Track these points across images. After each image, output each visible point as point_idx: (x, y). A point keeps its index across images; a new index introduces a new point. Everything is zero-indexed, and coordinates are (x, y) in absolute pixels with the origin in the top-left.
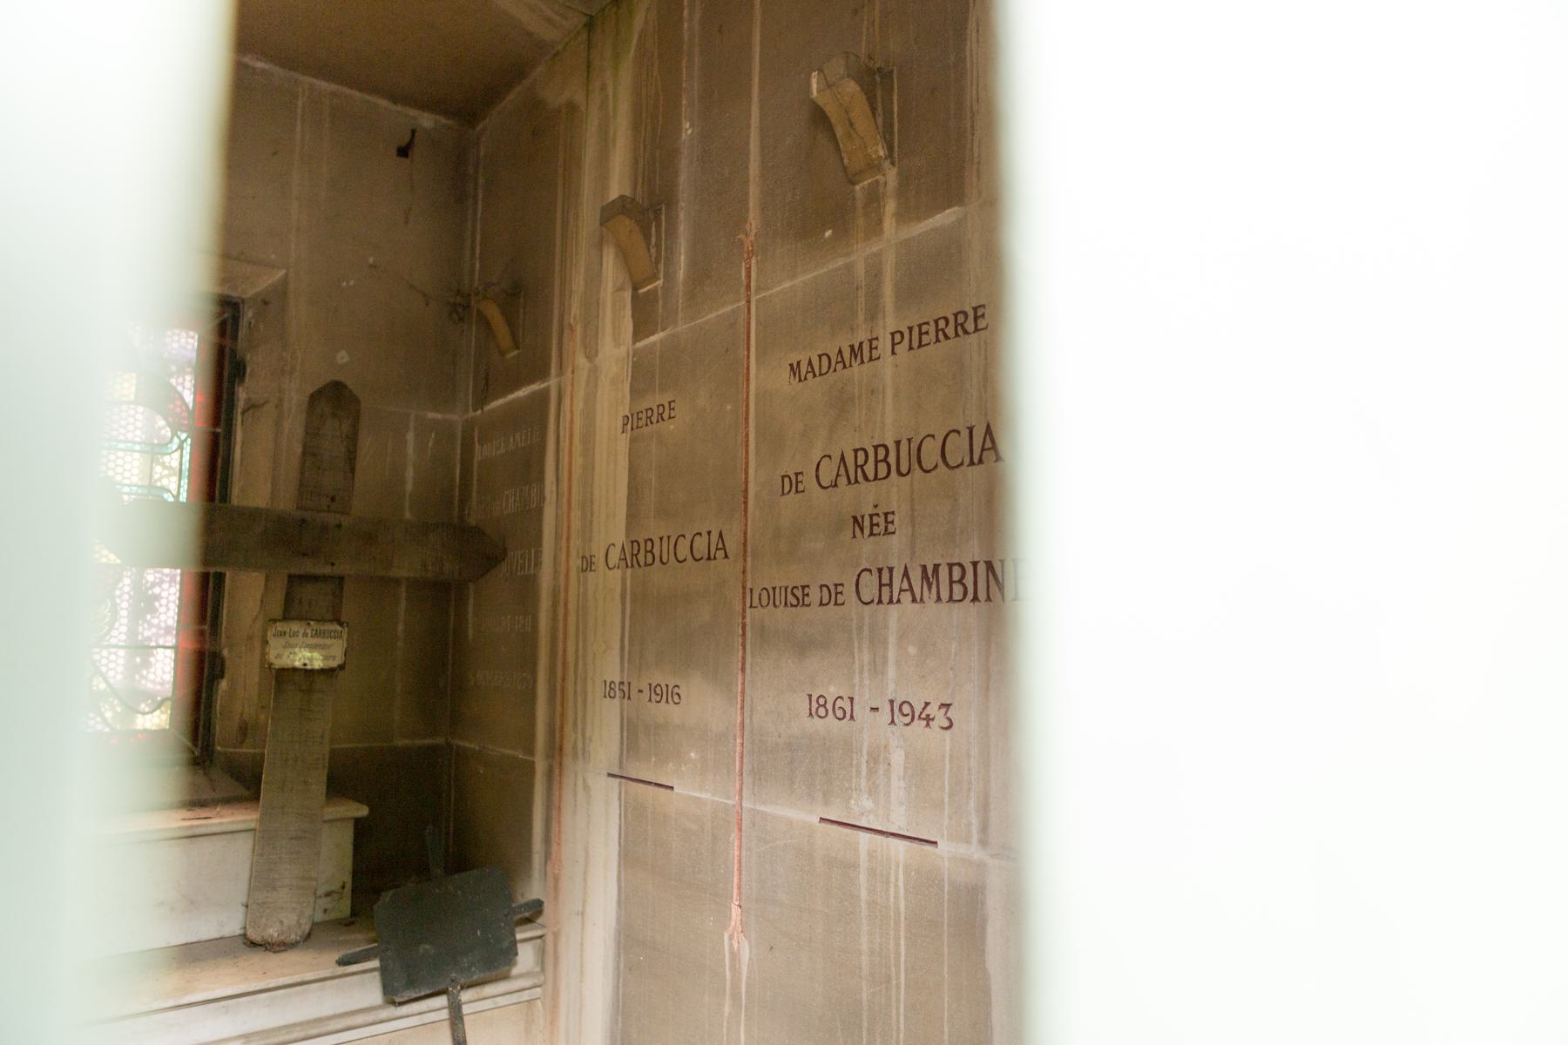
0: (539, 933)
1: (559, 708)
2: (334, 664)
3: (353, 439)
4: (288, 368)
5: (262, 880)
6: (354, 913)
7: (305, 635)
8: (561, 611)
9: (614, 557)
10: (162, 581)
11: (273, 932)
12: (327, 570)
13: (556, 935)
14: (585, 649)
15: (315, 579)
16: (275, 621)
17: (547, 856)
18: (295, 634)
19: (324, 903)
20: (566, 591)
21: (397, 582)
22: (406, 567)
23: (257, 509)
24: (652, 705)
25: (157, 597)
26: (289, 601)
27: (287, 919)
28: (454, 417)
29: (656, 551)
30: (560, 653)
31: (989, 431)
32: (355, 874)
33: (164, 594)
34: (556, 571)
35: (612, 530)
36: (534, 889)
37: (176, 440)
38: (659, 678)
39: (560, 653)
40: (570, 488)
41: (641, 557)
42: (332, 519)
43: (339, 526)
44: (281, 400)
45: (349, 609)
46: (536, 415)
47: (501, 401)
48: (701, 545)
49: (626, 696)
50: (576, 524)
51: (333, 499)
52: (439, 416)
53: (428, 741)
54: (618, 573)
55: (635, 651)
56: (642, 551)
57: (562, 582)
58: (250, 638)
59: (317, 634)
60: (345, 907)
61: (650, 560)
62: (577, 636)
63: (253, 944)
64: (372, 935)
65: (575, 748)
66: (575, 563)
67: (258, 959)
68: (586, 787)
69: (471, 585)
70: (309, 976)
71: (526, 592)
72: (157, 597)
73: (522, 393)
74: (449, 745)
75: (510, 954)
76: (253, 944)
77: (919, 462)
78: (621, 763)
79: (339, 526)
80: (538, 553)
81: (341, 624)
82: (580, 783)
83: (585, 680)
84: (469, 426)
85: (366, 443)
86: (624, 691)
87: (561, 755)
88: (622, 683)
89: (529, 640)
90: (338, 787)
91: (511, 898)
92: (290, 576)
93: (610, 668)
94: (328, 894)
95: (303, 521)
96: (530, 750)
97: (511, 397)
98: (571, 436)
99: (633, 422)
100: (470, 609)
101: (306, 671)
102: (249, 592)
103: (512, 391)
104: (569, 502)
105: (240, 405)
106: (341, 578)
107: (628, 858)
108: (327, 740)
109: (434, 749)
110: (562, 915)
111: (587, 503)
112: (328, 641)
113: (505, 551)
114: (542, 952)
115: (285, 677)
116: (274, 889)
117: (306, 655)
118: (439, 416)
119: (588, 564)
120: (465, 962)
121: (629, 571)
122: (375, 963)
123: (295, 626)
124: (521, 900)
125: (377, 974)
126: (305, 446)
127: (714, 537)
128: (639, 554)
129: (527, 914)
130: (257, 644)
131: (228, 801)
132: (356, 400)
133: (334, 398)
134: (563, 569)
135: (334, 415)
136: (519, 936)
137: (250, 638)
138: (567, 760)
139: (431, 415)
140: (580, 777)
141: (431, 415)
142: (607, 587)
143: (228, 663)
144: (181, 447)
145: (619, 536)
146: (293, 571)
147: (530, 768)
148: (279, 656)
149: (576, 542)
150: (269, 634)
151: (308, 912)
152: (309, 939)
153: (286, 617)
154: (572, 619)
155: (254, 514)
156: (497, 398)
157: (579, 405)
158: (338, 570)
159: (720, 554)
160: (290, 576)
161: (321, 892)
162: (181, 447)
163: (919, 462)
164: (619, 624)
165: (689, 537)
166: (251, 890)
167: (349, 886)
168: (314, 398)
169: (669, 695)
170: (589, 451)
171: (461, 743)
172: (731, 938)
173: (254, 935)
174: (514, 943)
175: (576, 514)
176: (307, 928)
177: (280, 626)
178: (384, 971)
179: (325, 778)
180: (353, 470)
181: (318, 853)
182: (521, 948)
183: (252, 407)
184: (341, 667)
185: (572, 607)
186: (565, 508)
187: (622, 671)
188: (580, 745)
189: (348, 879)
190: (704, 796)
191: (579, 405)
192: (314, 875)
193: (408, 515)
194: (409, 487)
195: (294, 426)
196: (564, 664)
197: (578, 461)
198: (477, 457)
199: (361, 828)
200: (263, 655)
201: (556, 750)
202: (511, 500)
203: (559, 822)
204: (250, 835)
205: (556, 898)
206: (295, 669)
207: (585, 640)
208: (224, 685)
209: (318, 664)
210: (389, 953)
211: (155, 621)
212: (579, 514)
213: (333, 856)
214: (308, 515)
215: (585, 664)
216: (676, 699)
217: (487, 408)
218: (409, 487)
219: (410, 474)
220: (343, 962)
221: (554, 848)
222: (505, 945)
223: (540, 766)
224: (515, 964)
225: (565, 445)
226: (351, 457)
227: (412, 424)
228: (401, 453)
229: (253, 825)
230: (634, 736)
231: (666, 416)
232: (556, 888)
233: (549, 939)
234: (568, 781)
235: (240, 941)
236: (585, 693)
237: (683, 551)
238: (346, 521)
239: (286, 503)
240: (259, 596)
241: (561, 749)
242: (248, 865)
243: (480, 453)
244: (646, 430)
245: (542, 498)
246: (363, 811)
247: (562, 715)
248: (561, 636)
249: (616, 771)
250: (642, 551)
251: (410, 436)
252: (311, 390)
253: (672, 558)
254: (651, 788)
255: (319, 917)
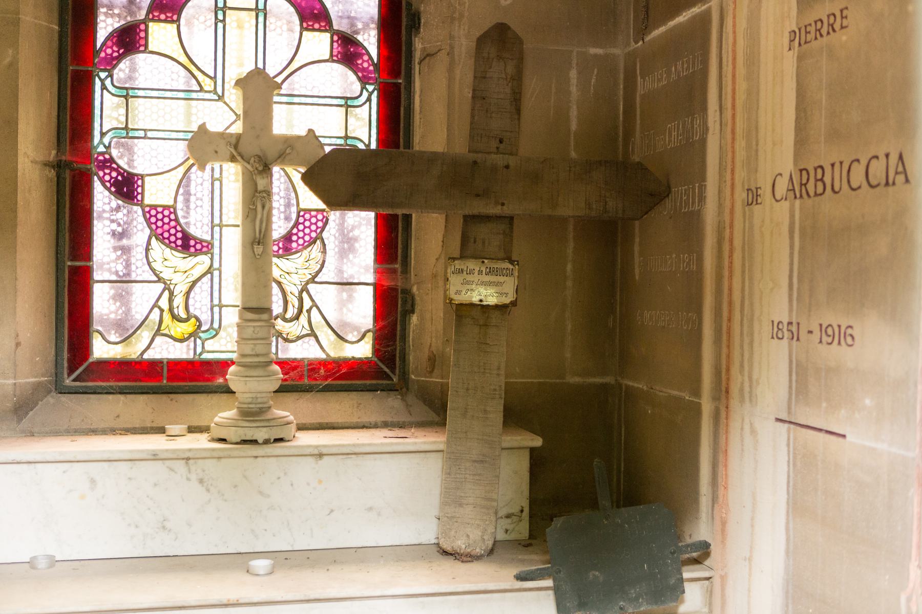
0: (706, 574)
1: (724, 350)
2: (507, 300)
3: (518, 78)
4: (457, 15)
5: (451, 498)
6: (531, 536)
7: (480, 272)
8: (726, 247)
9: (782, 186)
10: (360, 224)
11: (460, 544)
12: (497, 210)
13: (723, 578)
14: (751, 288)
15: (487, 218)
16: (454, 259)
17: (714, 500)
18: (471, 272)
19: (505, 523)
20: (731, 226)
21: (564, 220)
22: (573, 205)
23: (435, 154)
24: (823, 348)
25: (356, 239)
26: (465, 240)
27: (473, 534)
28: (616, 51)
29: (828, 179)
30: (726, 291)
31: (901, 157)
32: (533, 502)
33: (362, 236)
34: (720, 206)
35: (779, 159)
36: (701, 531)
37: (365, 94)
38: (830, 318)
39: (726, 291)
40: (734, 116)
41: (811, 187)
42: (499, 160)
43: (507, 167)
44: (452, 47)
45: (520, 249)
46: (698, 37)
47: (662, 29)
48: (877, 169)
49: (795, 337)
50: (741, 155)
51: (501, 141)
52: (599, 51)
53: (598, 380)
54: (786, 205)
55: (804, 289)
56: (812, 180)
57: (727, 219)
58: (435, 276)
59: (490, 272)
60: (523, 530)
61: (820, 189)
62: (743, 272)
63: (445, 553)
64: (547, 557)
65: (741, 390)
66: (741, 196)
67: (449, 565)
68: (753, 432)
69: (637, 223)
70: (491, 586)
71: (691, 225)
72: (356, 239)
73: (682, 18)
74: (620, 385)
75: (676, 591)
76: (445, 553)
77: (849, 181)
78: (789, 408)
79: (507, 167)
80: (703, 188)
81: (512, 262)
82: (747, 427)
83: (751, 321)
84: (631, 57)
85: (532, 86)
86: (792, 331)
87: (727, 398)
88: (790, 323)
89: (695, 279)
90: (514, 417)
91: (679, 538)
92: (466, 218)
93: (775, 304)
94: (508, 516)
95: (475, 162)
96: (697, 392)
97: (672, 24)
98: (734, 59)
99: (800, 37)
100: (636, 248)
101: (482, 306)
102: (431, 233)
103: (672, 17)
104: (733, 132)
105: (417, 55)
106: (511, 218)
107: (797, 507)
108: (502, 372)
109: (604, 386)
110: (729, 557)
111: (753, 130)
112: (501, 279)
113: (669, 187)
114: (710, 593)
115: (464, 312)
116: (461, 505)
117: (486, 294)
118: (599, 51)
119: (754, 197)
120: (633, 593)
121: (798, 202)
122: (549, 583)
123: (471, 264)
124: (689, 541)
125: (551, 593)
126: (474, 90)
127: (894, 159)
128: (809, 183)
129: (695, 555)
130: (441, 283)
131: (422, 425)
132: (519, 41)
133: (499, 40)
134: (728, 203)
135: (499, 58)
136: (686, 575)
137: (435, 276)
138: (734, 403)
139: (593, 51)
140: (747, 421)
141: (593, 51)
142: (776, 218)
143: (417, 299)
144: (369, 99)
145: (787, 165)
146: (467, 212)
147: (696, 410)
148: (458, 292)
149: (740, 174)
150: (449, 271)
151: (491, 529)
152: (491, 552)
153: (462, 257)
154: (737, 255)
155: (433, 158)
156: (657, 27)
157: (742, 24)
158: (507, 210)
159: (901, 178)
160: (466, 218)
161: (502, 513)
162: (369, 99)
163: (849, 181)
164: (787, 260)
165: (864, 162)
166: (444, 504)
167: (526, 510)
168: (481, 41)
169: (840, 336)
170: (753, 76)
171: (631, 384)
172: (909, 600)
173: (447, 546)
174: (681, 580)
175: (741, 144)
176: (490, 544)
177: (458, 264)
178: (557, 589)
179: (502, 408)
180: (518, 111)
181: (498, 477)
182: (687, 586)
183: (428, 56)
184: (514, 304)
185: (737, 243)
186: (729, 136)
187: (791, 310)
188: (747, 389)
189: (526, 504)
190: (882, 446)
191: (742, 24)
192: (495, 497)
193: (573, 154)
194: (574, 126)
195: (465, 73)
196: (730, 303)
197: (742, 86)
198: (640, 91)
199: (537, 460)
200: (445, 291)
201: (722, 392)
202: (674, 134)
203: (726, 466)
204: (440, 455)
205: (723, 542)
206: (472, 305)
207: (751, 279)
208: (414, 319)
209: (492, 300)
210: (562, 575)
211: (114, 174)
212: (743, 144)
213: (512, 481)
214: (479, 157)
215: (752, 304)
216: (849, 340)
217: (648, 38)
218: (574, 126)
219: (574, 113)
220: (521, 578)
221: (721, 491)
222: (672, 581)
223: (707, 407)
224: (682, 601)
225: (728, 69)
226: (517, 99)
227: (574, 62)
228: (563, 92)
229: (442, 447)
230: (803, 380)
231: (837, 26)
232: (723, 531)
233: (717, 581)
234: (735, 425)
235: (435, 549)
236: (751, 334)
237: (858, 177)
238: (512, 161)
239: (461, 148)
240: (440, 236)
241: (727, 392)
242: (439, 481)
243: (642, 87)
244: (815, 44)
245: (706, 130)
246: (538, 442)
247: (728, 356)
248: (726, 273)
249: (784, 416)
250: (812, 180)
251: (573, 74)
252: (478, 34)
253: (845, 186)
254: (821, 435)
255: (501, 536)
